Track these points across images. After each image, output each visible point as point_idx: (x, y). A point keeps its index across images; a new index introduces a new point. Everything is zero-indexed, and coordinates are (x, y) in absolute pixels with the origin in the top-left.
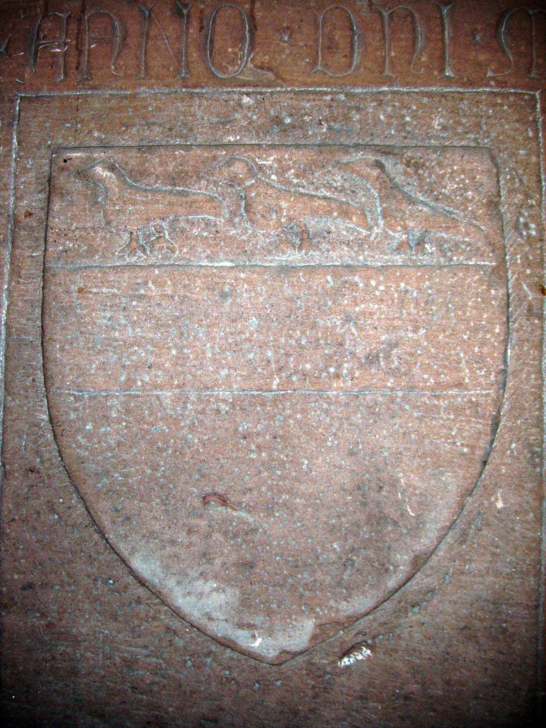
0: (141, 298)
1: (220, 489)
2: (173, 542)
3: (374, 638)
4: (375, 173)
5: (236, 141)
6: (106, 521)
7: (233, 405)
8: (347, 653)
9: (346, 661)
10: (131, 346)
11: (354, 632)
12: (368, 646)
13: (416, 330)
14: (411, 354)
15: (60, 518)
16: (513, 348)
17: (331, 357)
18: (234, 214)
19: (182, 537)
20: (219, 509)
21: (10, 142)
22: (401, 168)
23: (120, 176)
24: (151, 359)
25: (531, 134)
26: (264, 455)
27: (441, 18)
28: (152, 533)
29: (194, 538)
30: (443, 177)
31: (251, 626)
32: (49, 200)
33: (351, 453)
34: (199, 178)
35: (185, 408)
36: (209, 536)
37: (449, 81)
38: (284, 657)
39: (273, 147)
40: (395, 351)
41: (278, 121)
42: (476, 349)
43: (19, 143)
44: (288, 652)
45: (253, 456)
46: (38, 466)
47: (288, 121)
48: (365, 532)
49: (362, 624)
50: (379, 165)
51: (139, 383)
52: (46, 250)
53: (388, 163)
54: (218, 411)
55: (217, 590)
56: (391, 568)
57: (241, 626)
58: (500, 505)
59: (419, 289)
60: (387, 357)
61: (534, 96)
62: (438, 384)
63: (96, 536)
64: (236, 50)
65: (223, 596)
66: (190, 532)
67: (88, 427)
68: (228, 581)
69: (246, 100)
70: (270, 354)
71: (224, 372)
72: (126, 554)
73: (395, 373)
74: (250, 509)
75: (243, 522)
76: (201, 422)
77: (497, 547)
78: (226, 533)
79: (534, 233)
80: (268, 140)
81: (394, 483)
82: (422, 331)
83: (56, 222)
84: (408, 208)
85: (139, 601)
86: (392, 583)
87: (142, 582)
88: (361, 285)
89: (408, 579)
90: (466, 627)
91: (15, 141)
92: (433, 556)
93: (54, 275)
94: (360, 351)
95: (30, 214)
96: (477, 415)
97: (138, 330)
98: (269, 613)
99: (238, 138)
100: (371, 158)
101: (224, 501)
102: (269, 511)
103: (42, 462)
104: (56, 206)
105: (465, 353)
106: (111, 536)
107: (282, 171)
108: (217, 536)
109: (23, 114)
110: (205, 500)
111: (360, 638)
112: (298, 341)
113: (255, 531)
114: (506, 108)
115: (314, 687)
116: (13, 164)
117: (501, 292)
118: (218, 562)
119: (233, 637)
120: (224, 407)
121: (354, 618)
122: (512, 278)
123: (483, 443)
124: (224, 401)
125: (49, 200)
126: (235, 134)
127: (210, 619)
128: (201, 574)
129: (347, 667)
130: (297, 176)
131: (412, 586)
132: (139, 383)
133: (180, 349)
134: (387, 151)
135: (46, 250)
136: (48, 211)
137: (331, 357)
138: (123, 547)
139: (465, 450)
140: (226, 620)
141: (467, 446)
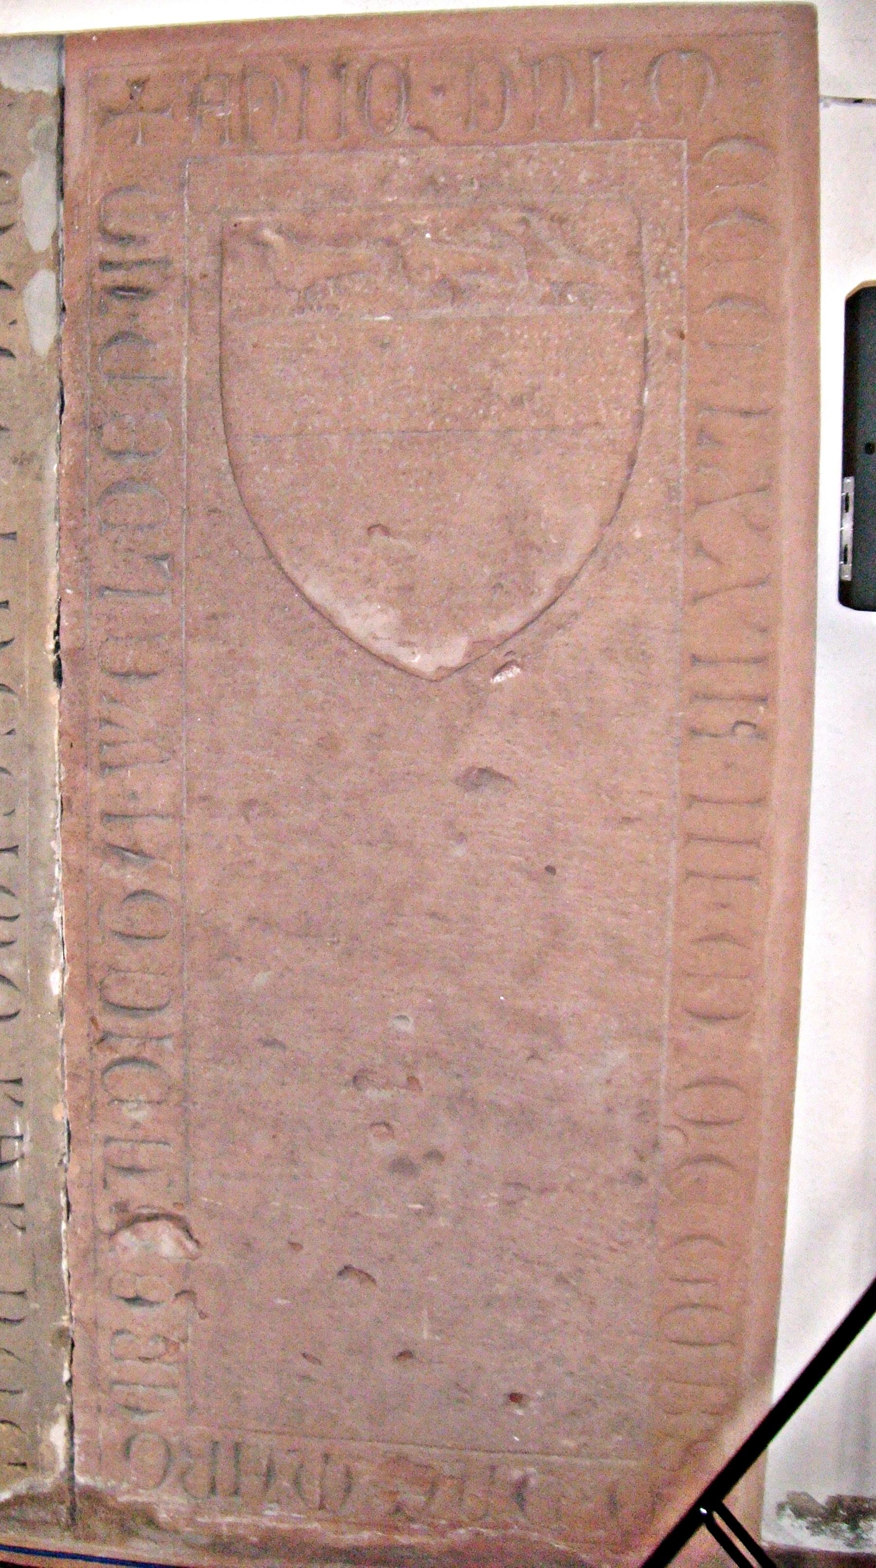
0: (309, 351)
1: (383, 520)
2: (341, 569)
3: (524, 656)
4: (521, 229)
5: (393, 201)
6: (282, 552)
7: (393, 445)
8: (498, 671)
9: (498, 679)
10: (303, 395)
11: (505, 653)
12: (518, 666)
13: (557, 374)
14: (553, 396)
15: (240, 553)
16: (650, 390)
17: (480, 400)
18: (392, 271)
19: (350, 564)
20: (382, 538)
21: (182, 207)
22: (545, 223)
23: (288, 238)
24: (321, 406)
25: (675, 184)
26: (421, 489)
27: (591, 68)
28: (323, 561)
29: (360, 566)
30: (585, 230)
31: (410, 644)
32: (222, 262)
33: (499, 487)
34: (360, 238)
35: (350, 449)
36: (372, 563)
37: (597, 136)
38: (443, 673)
39: (428, 207)
40: (537, 394)
41: (432, 181)
42: (613, 391)
43: (191, 208)
44: (446, 669)
45: (412, 490)
46: (219, 507)
47: (442, 180)
48: (512, 558)
49: (510, 646)
50: (525, 222)
51: (310, 428)
52: (221, 309)
53: (534, 220)
54: (380, 451)
55: (381, 610)
56: (536, 590)
57: (402, 643)
58: (638, 535)
59: (560, 338)
60: (531, 399)
61: (679, 146)
62: (578, 423)
63: (273, 568)
64: (392, 109)
65: (385, 617)
66: (357, 560)
67: (265, 469)
68: (391, 603)
69: (402, 160)
70: (425, 399)
71: (385, 417)
72: (299, 581)
73: (536, 414)
74: (408, 537)
75: (403, 549)
76: (365, 460)
77: (636, 574)
78: (388, 560)
79: (674, 280)
80: (423, 200)
81: (538, 514)
82: (562, 375)
83: (230, 283)
84: (550, 263)
85: (312, 626)
86: (537, 603)
87: (314, 608)
88: (507, 334)
89: (554, 602)
90: (607, 649)
91: (186, 205)
92: (576, 581)
93: (230, 333)
94: (506, 394)
95: (205, 276)
96: (614, 452)
97: (308, 380)
98: (428, 631)
99: (396, 198)
100: (518, 215)
101: (386, 531)
102: (427, 538)
103: (223, 503)
104: (230, 268)
105: (603, 395)
106: (286, 566)
107: (435, 230)
108: (381, 563)
109: (192, 179)
110: (370, 530)
111: (509, 659)
112: (450, 386)
113: (411, 558)
114: (651, 158)
115: (470, 703)
116: (187, 228)
117: (639, 338)
118: (381, 586)
119: (396, 655)
120: (385, 447)
121: (506, 638)
122: (651, 324)
123: (619, 477)
124: (385, 441)
125: (222, 262)
126: (391, 196)
127: (375, 638)
128: (366, 598)
129: (500, 684)
130: (449, 234)
131: (557, 608)
132: (310, 428)
133: (346, 396)
134: (532, 209)
135: (221, 309)
136: (220, 271)
137: (480, 400)
138: (298, 576)
139: (603, 483)
140: (389, 639)
141: (605, 480)
